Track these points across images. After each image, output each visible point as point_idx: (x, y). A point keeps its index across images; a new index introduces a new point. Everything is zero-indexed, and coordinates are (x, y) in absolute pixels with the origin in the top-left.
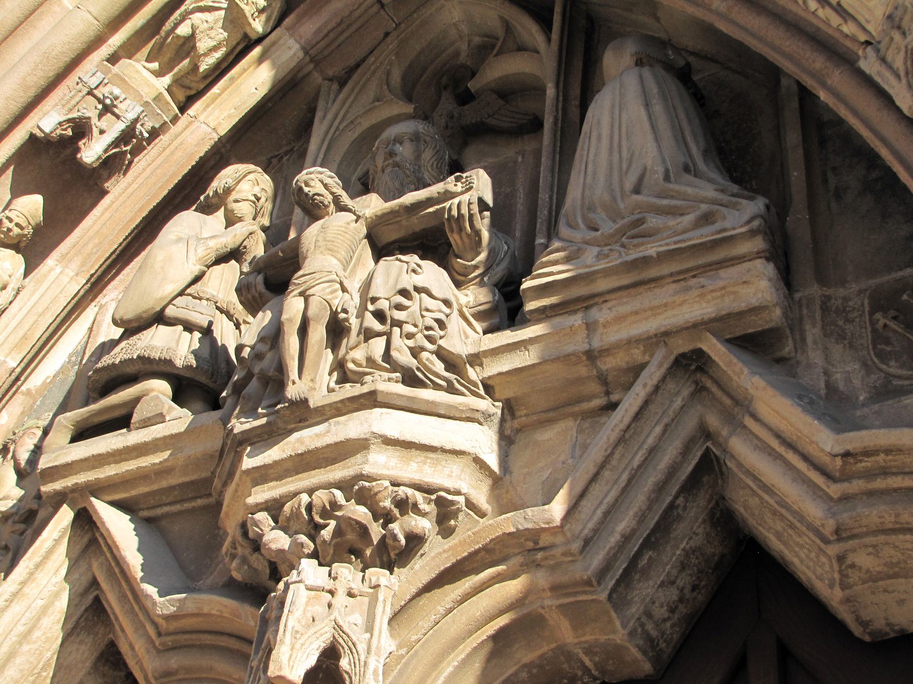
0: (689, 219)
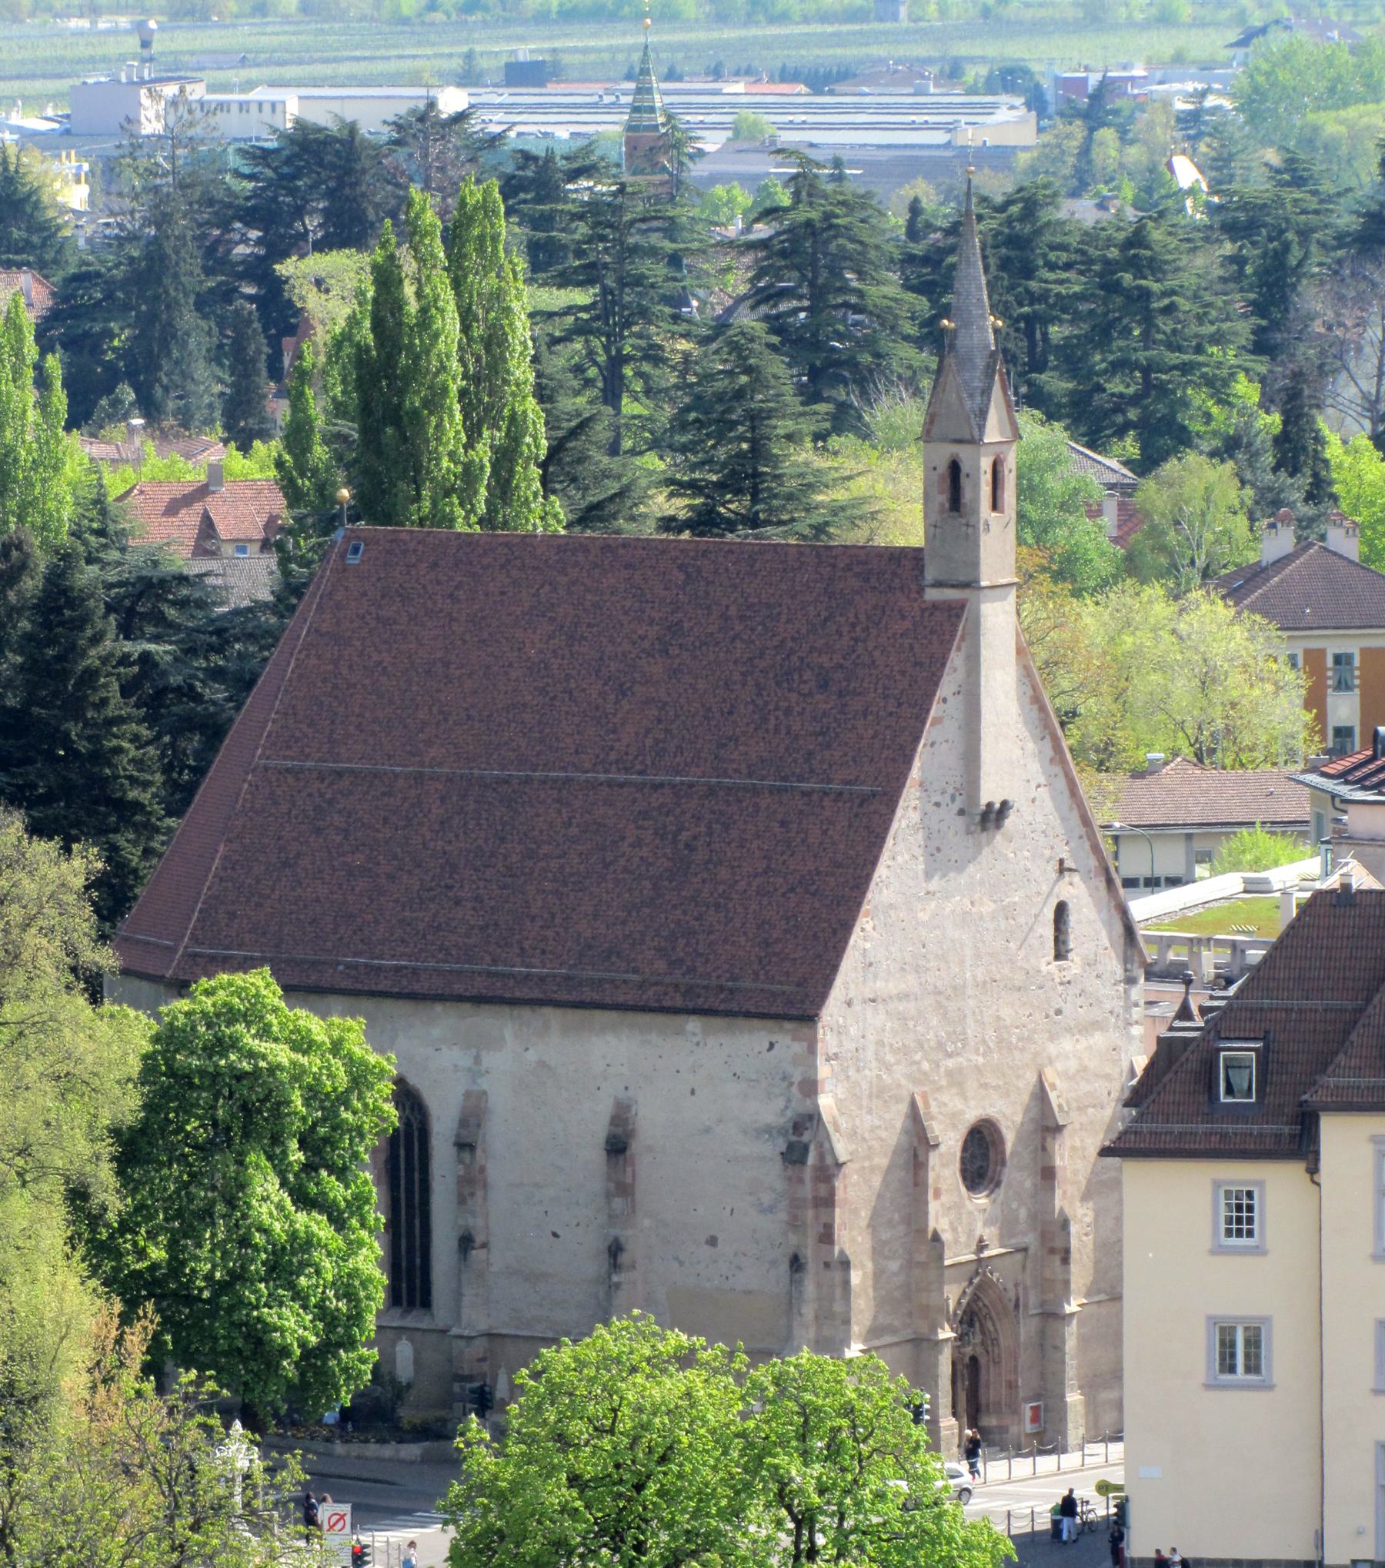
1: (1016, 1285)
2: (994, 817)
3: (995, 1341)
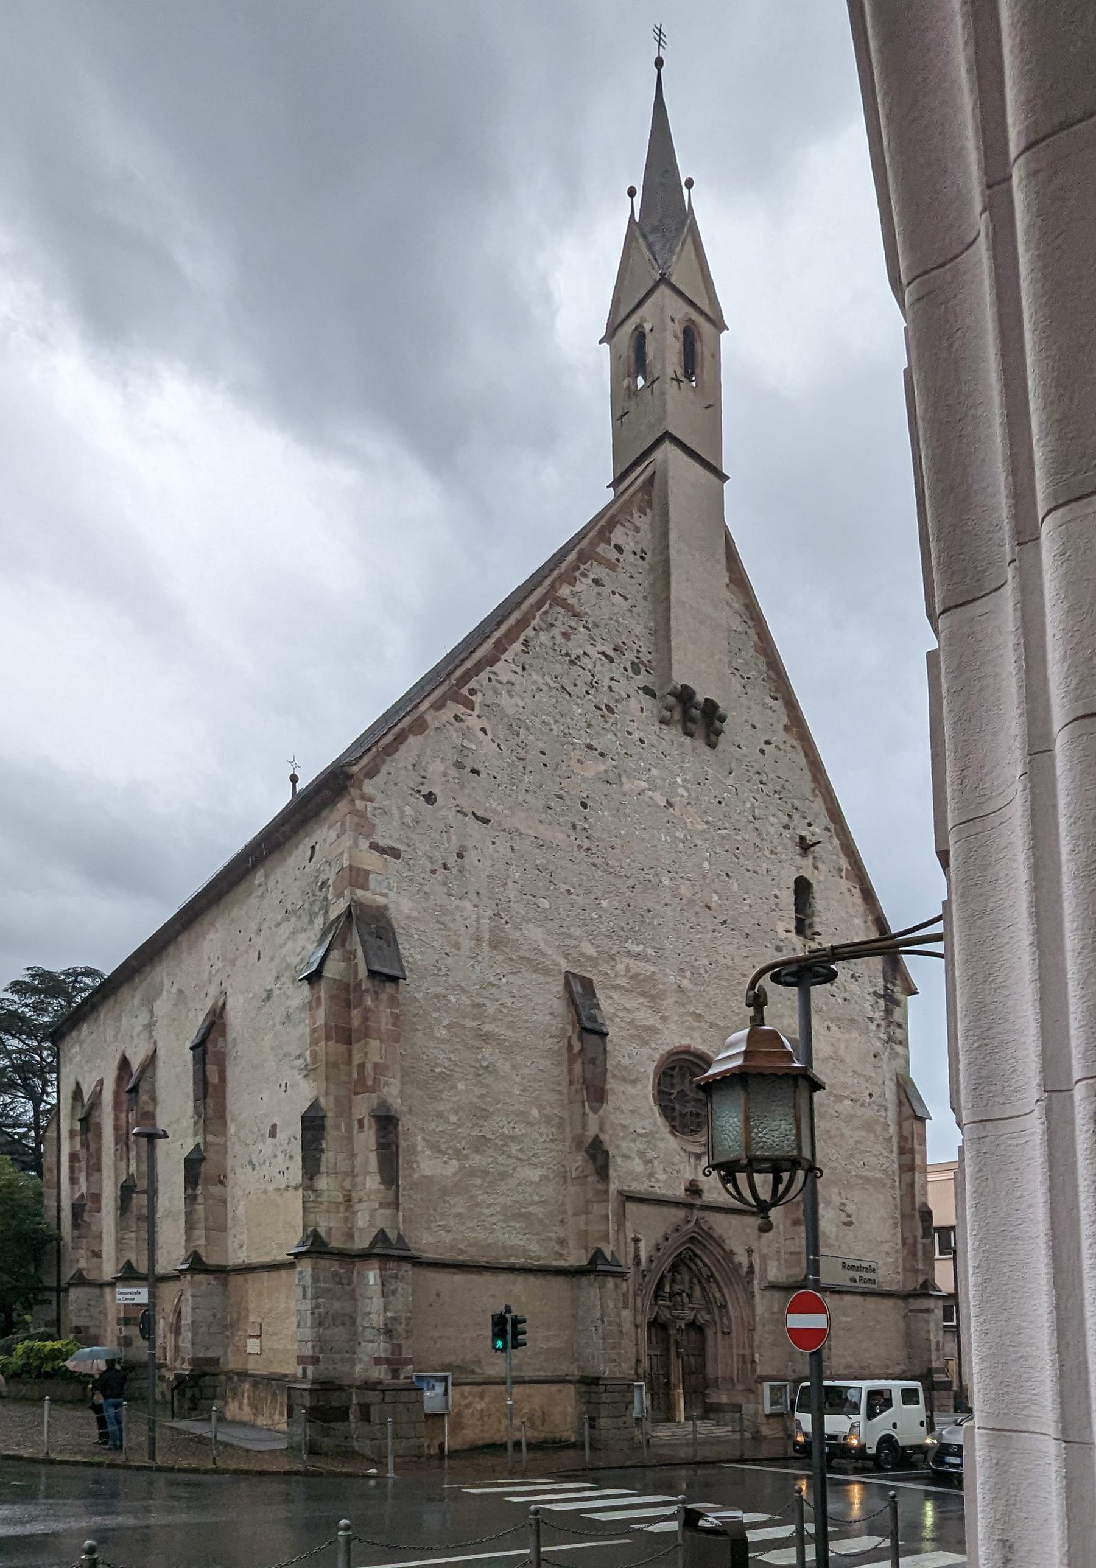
1: (750, 1252)
2: (698, 717)
3: (723, 1307)
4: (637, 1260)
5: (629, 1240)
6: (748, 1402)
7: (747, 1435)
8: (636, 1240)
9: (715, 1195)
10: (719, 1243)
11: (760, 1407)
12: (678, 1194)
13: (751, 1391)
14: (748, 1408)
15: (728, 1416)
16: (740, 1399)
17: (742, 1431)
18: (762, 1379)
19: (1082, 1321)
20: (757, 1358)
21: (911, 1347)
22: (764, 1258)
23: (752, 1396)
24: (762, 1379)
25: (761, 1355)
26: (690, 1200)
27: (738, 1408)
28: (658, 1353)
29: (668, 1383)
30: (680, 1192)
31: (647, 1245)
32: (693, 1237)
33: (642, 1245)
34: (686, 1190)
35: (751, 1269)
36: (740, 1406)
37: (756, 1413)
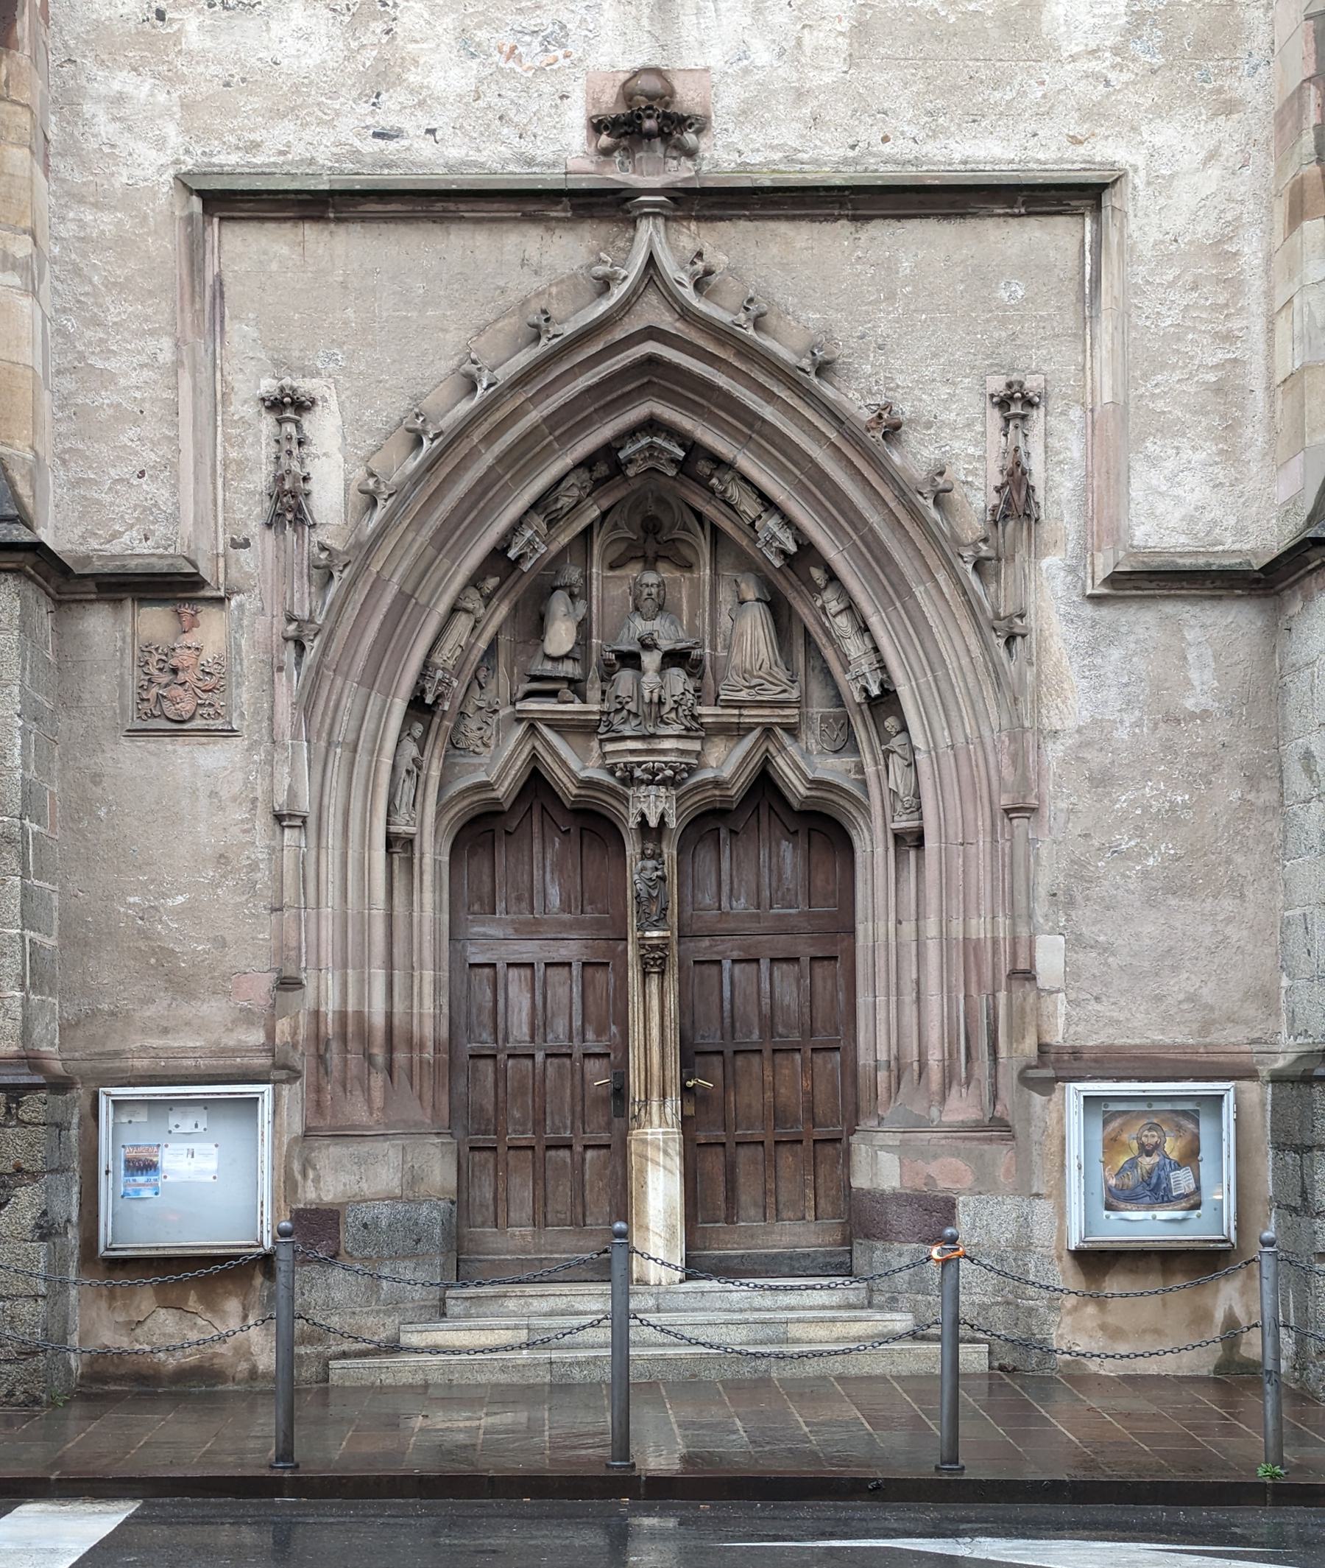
0: (779, 689)
1: (1015, 404)
4: (288, 506)
5: (244, 408)
6: (985, 1184)
7: (974, 1357)
8: (287, 406)
9: (789, 135)
10: (808, 379)
11: (1043, 1208)
12: (544, 151)
13: (998, 1127)
14: (983, 1221)
15: (901, 1253)
16: (948, 1173)
17: (954, 1332)
18: (1053, 1067)
19: (1135, 1540)
20: (1050, 957)
21: (174, 486)
22: (1113, 439)
23: (1002, 1156)
24: (1053, 1067)
25: (1076, 942)
26: (619, 174)
27: (935, 1214)
28: (571, 950)
29: (620, 1093)
30: (563, 147)
31: (352, 424)
32: (652, 360)
33: (324, 428)
34: (598, 126)
35: (1016, 501)
36: (947, 1209)
37: (1023, 1245)
